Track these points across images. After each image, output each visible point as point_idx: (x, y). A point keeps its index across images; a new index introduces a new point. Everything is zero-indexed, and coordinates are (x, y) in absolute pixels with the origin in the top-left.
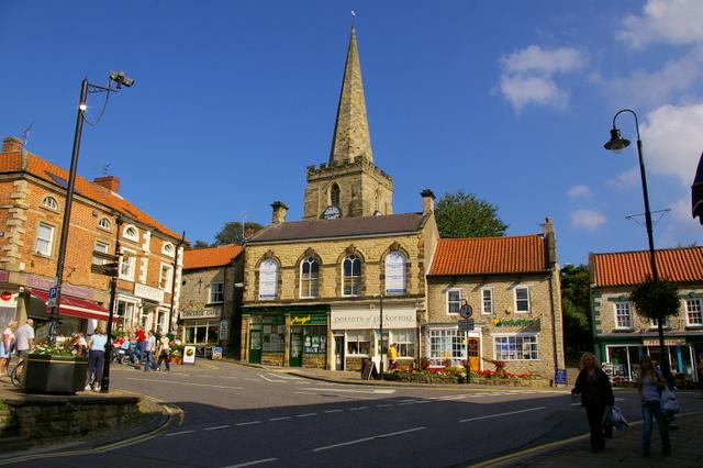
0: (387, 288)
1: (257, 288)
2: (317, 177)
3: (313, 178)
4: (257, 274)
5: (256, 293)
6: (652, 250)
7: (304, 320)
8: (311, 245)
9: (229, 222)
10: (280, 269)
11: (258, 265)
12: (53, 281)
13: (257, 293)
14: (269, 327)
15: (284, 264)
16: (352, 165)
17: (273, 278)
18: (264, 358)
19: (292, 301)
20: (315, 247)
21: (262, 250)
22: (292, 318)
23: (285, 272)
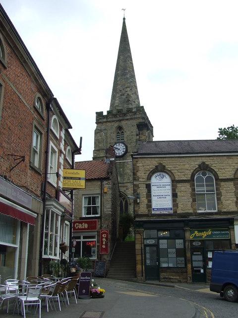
0: (154, 206)
1: (150, 201)
2: (105, 120)
3: (100, 121)
4: (149, 187)
5: (149, 206)
6: (44, 200)
7: (204, 234)
8: (204, 160)
9: (225, 125)
10: (175, 182)
11: (149, 178)
12: (141, 165)
13: (150, 206)
14: (182, 247)
15: (177, 179)
16: (135, 113)
17: (168, 190)
18: (162, 275)
19: (191, 214)
20: (208, 162)
21: (152, 163)
22: (192, 232)
23: (179, 185)
